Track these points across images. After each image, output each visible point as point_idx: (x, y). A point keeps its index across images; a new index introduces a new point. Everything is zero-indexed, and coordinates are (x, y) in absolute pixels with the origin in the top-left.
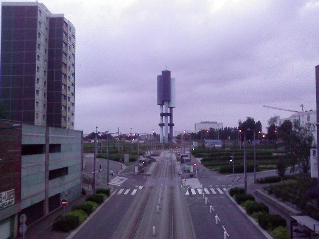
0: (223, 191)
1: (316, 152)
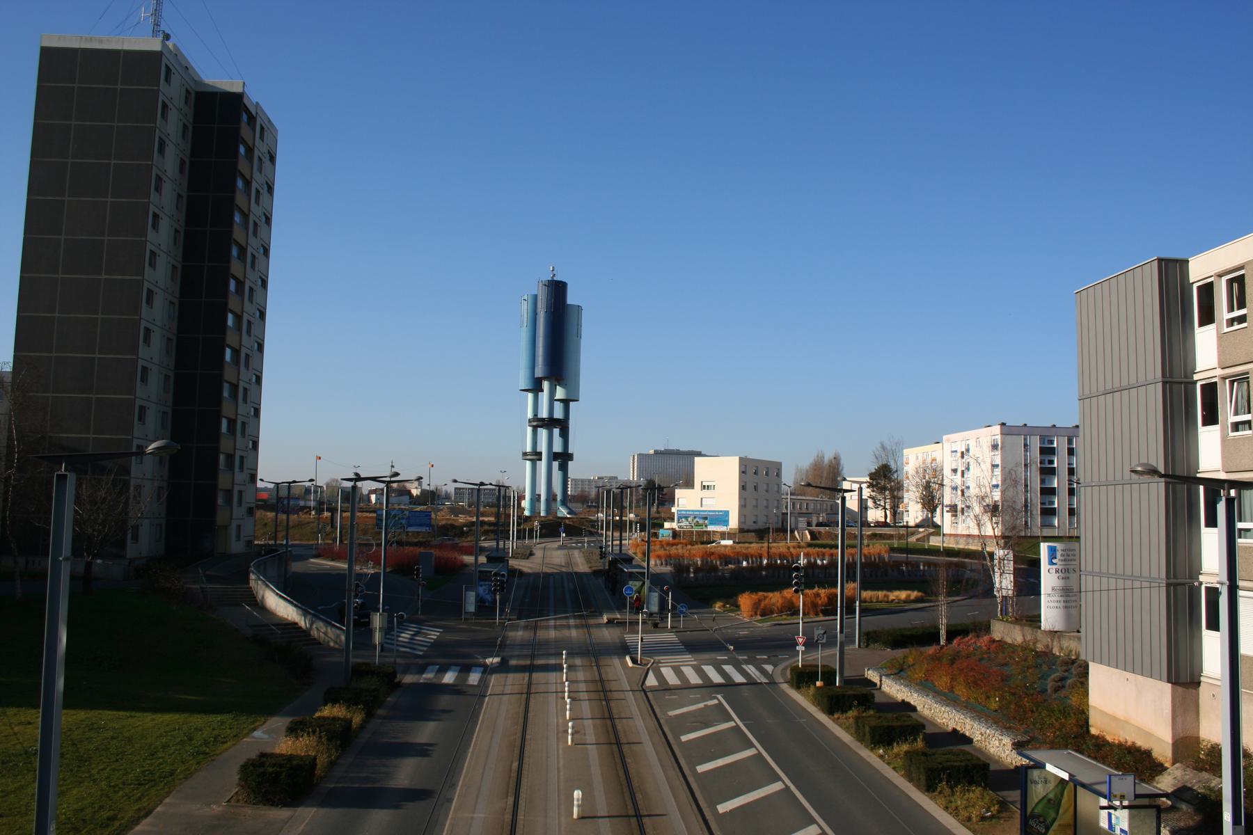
0: (764, 672)
1: (1059, 554)
